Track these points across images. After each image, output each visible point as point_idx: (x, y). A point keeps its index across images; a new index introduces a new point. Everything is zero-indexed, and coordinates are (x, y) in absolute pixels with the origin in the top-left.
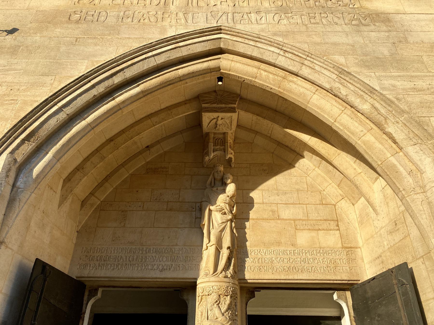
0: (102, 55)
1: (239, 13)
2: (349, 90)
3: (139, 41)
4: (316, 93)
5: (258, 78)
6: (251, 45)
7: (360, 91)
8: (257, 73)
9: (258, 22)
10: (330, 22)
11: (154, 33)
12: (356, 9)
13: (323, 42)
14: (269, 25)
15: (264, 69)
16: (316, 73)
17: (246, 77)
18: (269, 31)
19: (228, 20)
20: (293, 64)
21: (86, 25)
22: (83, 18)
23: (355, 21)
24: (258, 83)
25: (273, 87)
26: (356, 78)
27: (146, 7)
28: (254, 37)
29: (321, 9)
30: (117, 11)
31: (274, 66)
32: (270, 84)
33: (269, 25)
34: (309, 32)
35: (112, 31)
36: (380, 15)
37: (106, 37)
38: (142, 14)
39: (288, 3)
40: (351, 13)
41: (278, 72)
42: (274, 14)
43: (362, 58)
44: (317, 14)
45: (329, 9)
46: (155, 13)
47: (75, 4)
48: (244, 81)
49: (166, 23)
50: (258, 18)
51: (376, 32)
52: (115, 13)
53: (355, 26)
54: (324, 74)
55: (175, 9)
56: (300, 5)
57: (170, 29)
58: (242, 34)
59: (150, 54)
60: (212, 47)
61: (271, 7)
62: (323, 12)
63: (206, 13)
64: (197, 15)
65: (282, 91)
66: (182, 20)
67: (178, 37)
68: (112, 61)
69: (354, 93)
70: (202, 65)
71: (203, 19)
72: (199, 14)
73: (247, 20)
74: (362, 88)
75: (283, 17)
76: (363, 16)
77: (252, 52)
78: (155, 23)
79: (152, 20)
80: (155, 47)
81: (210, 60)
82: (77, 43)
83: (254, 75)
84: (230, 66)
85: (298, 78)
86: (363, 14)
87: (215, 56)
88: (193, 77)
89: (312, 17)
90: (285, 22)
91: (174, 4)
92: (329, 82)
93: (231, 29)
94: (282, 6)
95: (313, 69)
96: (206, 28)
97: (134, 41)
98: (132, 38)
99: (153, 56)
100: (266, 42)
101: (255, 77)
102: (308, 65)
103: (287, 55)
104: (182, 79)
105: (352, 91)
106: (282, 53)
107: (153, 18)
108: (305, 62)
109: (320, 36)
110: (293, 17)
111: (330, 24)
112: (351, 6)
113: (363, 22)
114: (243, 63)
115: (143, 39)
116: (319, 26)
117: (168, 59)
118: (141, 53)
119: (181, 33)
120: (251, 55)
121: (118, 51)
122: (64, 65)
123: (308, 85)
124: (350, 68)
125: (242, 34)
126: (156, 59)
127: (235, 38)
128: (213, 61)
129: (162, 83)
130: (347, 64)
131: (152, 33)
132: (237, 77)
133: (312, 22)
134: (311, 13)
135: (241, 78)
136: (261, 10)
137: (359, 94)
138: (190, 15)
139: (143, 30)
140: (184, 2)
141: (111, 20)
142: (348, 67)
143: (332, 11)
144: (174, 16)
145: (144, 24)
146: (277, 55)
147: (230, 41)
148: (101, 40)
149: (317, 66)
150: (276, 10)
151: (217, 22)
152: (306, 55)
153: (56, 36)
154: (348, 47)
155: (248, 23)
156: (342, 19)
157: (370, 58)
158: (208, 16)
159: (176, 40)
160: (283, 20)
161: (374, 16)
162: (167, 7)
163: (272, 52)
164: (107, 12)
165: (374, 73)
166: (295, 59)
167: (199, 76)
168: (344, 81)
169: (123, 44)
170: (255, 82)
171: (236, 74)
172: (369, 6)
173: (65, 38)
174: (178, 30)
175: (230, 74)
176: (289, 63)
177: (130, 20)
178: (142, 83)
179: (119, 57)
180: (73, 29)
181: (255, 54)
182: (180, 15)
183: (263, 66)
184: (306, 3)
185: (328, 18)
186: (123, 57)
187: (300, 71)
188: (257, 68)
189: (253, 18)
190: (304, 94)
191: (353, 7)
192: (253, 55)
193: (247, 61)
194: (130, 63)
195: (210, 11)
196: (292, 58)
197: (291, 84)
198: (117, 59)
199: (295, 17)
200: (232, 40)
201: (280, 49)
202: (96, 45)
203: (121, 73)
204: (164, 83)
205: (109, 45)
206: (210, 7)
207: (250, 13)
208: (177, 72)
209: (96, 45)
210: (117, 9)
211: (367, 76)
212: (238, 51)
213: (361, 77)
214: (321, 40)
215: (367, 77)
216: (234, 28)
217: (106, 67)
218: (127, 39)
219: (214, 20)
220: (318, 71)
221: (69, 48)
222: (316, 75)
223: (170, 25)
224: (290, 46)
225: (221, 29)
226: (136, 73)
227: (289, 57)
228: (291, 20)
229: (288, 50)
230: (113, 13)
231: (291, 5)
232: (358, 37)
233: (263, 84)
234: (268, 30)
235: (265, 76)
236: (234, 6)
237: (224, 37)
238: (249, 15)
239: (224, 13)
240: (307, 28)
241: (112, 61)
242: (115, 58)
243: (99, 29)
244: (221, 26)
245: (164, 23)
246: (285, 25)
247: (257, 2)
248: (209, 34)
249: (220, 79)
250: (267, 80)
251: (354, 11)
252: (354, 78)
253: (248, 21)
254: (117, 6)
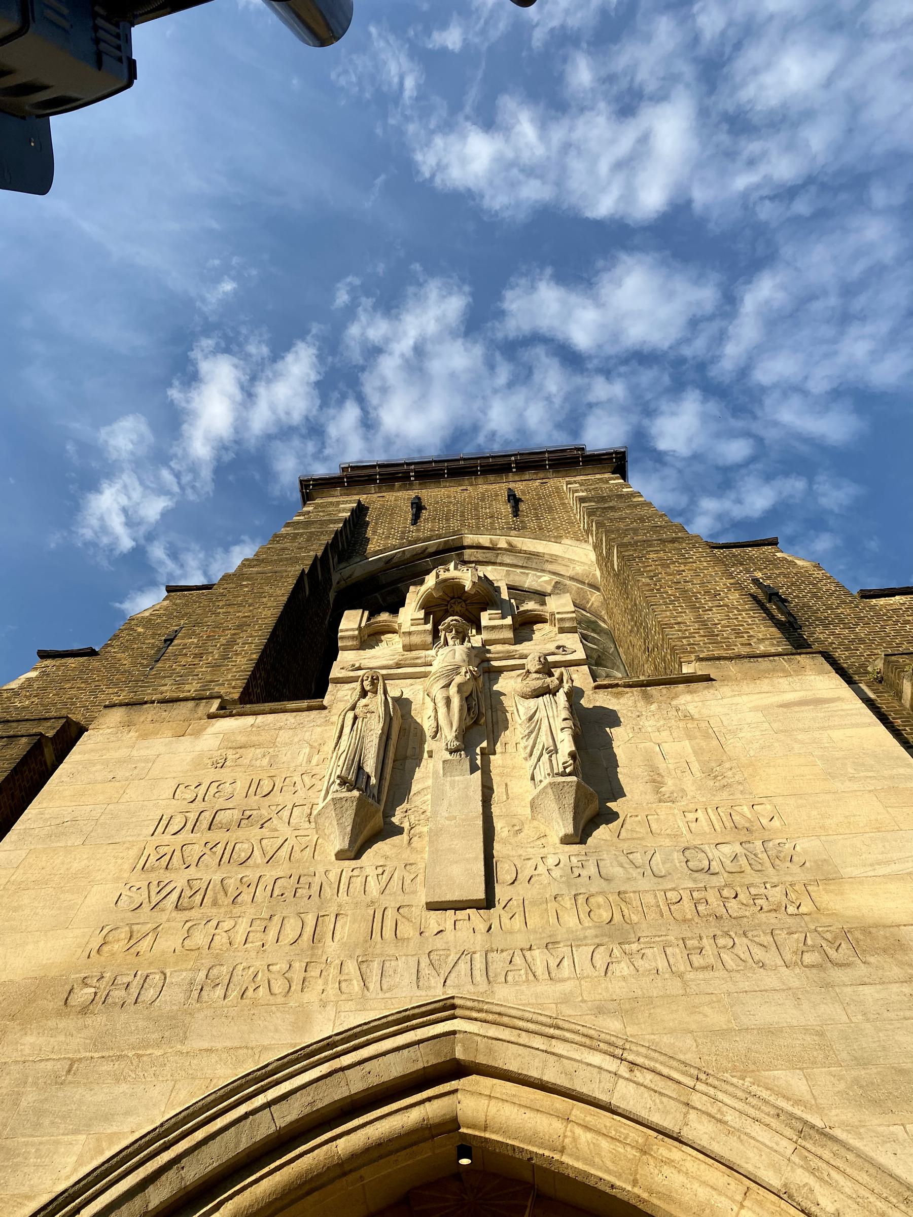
0: (128, 1113)
1: (502, 951)
2: (842, 1196)
3: (234, 1059)
4: (746, 1203)
5: (568, 1151)
6: (537, 1049)
7: (872, 1199)
8: (565, 1137)
9: (553, 975)
10: (743, 961)
11: (276, 1030)
12: (806, 918)
13: (733, 1025)
14: (583, 982)
15: (581, 1122)
16: (730, 1135)
17: (535, 1149)
18: (583, 1001)
19: (473, 973)
20: (660, 1106)
21: (105, 1019)
22: (101, 996)
23: (810, 953)
24: (572, 1167)
25: (618, 1183)
26: (850, 1153)
27: (264, 951)
28: (542, 1024)
29: (713, 924)
30: (190, 970)
31: (608, 1108)
32: (605, 1171)
33: (583, 982)
34: (693, 997)
35: (169, 1031)
36: (873, 930)
37: (148, 1052)
38: (253, 972)
39: (626, 912)
40: (794, 930)
41: (622, 1130)
42: (592, 948)
43: (854, 1073)
44: (705, 940)
45: (734, 921)
46: (285, 967)
47: (89, 957)
48: (531, 1159)
49: (311, 996)
50: (553, 964)
51: (875, 984)
52: (184, 974)
53: (814, 971)
54: (754, 1138)
55: (338, 952)
56: (658, 916)
57: (320, 1013)
58: (510, 1016)
59: (260, 1100)
60: (433, 1061)
61: (585, 929)
62: (721, 933)
63: (415, 959)
64: (393, 963)
65: (645, 1195)
66: (355, 982)
67: (338, 1041)
68: (151, 1135)
69: (856, 1206)
70: (405, 1119)
71: (408, 977)
72: (399, 962)
73: (523, 972)
74: (878, 1188)
75: (618, 955)
76: (829, 936)
77: (543, 1069)
78: (283, 999)
79: (276, 989)
80: (275, 1077)
81: (429, 1099)
82: (70, 1078)
83: (558, 1144)
84: (486, 1116)
85: (684, 1148)
86: (827, 931)
87: (441, 1086)
88: (381, 1157)
89: (694, 948)
90: (622, 968)
91: (336, 939)
92: (778, 1171)
93: (481, 1006)
94: (612, 923)
95: (720, 1121)
96: (413, 1008)
97: (221, 1060)
98: (217, 1050)
99: (268, 1105)
100: (577, 1038)
101: (560, 1148)
102: (703, 1109)
103: (639, 1076)
104: (347, 1168)
105: (850, 1197)
106: (623, 1070)
107: (280, 983)
108: (694, 1098)
109: (724, 1006)
110: (643, 951)
111: (745, 967)
112: (791, 909)
113: (832, 953)
114: (522, 1103)
115: (245, 1051)
116: (716, 974)
117: (308, 1110)
118: (235, 1101)
119: (346, 1028)
120: (541, 1080)
121: (175, 1097)
122: (18, 1155)
123: (717, 1175)
124: (826, 1112)
125: (510, 1016)
126: (274, 1115)
127: (493, 1031)
128: (436, 1103)
129: (289, 1189)
130: (815, 1100)
131: (272, 1028)
132: (509, 1148)
133: (696, 964)
134: (690, 939)
135: (522, 1150)
136: (559, 938)
137: (874, 1209)
138: (376, 966)
139: (249, 1020)
140: (362, 929)
141: (173, 997)
142: (819, 1109)
143: (743, 929)
144: (333, 971)
145: (254, 1003)
146: (613, 1078)
147: (479, 1039)
148: (135, 1062)
149: (732, 1111)
150: (596, 936)
151: (445, 982)
152: (691, 1076)
153: (19, 1059)
154: (808, 1038)
155: (527, 980)
156: (774, 948)
157: (879, 1073)
158: (422, 965)
159: (334, 1050)
160: (619, 962)
161: (858, 934)
162: (318, 948)
163: (596, 1070)
164: (165, 974)
165: (903, 1125)
166: (664, 1091)
167: (399, 1154)
168: (820, 1164)
169: (191, 1072)
170: (562, 1163)
171: (504, 1141)
172: (837, 907)
173: (43, 1064)
174: (343, 1014)
175: (487, 1139)
176: (650, 1103)
177: (220, 991)
178: (230, 1198)
179: (173, 1120)
180: (68, 1034)
181: (550, 1076)
182: (351, 968)
183: (579, 1111)
184: (672, 907)
185: (735, 950)
186: (185, 1117)
187: (685, 1129)
188: (562, 1119)
189: (539, 963)
190: (712, 1206)
191: (796, 911)
192: (545, 1078)
193: (532, 1097)
194: (200, 1135)
195: (427, 952)
196: (656, 1088)
197: (667, 1170)
198: (165, 1127)
199: (648, 952)
200: (485, 1037)
201: (618, 1058)
202: (118, 1081)
203: (171, 1173)
204: (295, 1189)
205: (154, 1078)
206: (427, 939)
207: (530, 949)
208: (333, 1148)
209: (118, 1079)
210: (192, 963)
211: (885, 1139)
212: (505, 1068)
213: (865, 1143)
214: (729, 1021)
215: (884, 1142)
216: (487, 1003)
217: (128, 1159)
218: (205, 1054)
219: (438, 978)
220: (734, 1128)
221: (47, 1094)
222: (733, 1141)
223: (321, 1000)
224: (643, 1050)
225: (454, 1007)
226: (215, 1165)
227: (645, 1084)
228: (639, 963)
229: (640, 1060)
230: (178, 977)
231: (635, 918)
232: (830, 1005)
233: (585, 1171)
234: (580, 998)
235: (589, 1145)
236: (488, 931)
237: (463, 1030)
238: (527, 954)
239: (463, 953)
240: (685, 984)
241: (151, 1135)
242: (162, 1125)
243: (137, 1028)
244: (453, 998)
245: (307, 997)
246: (624, 978)
247: (546, 914)
248: (423, 1022)
249: (464, 1151)
250: (597, 1160)
251: (803, 924)
252: (843, 1152)
253: (527, 974)
254: (193, 953)
